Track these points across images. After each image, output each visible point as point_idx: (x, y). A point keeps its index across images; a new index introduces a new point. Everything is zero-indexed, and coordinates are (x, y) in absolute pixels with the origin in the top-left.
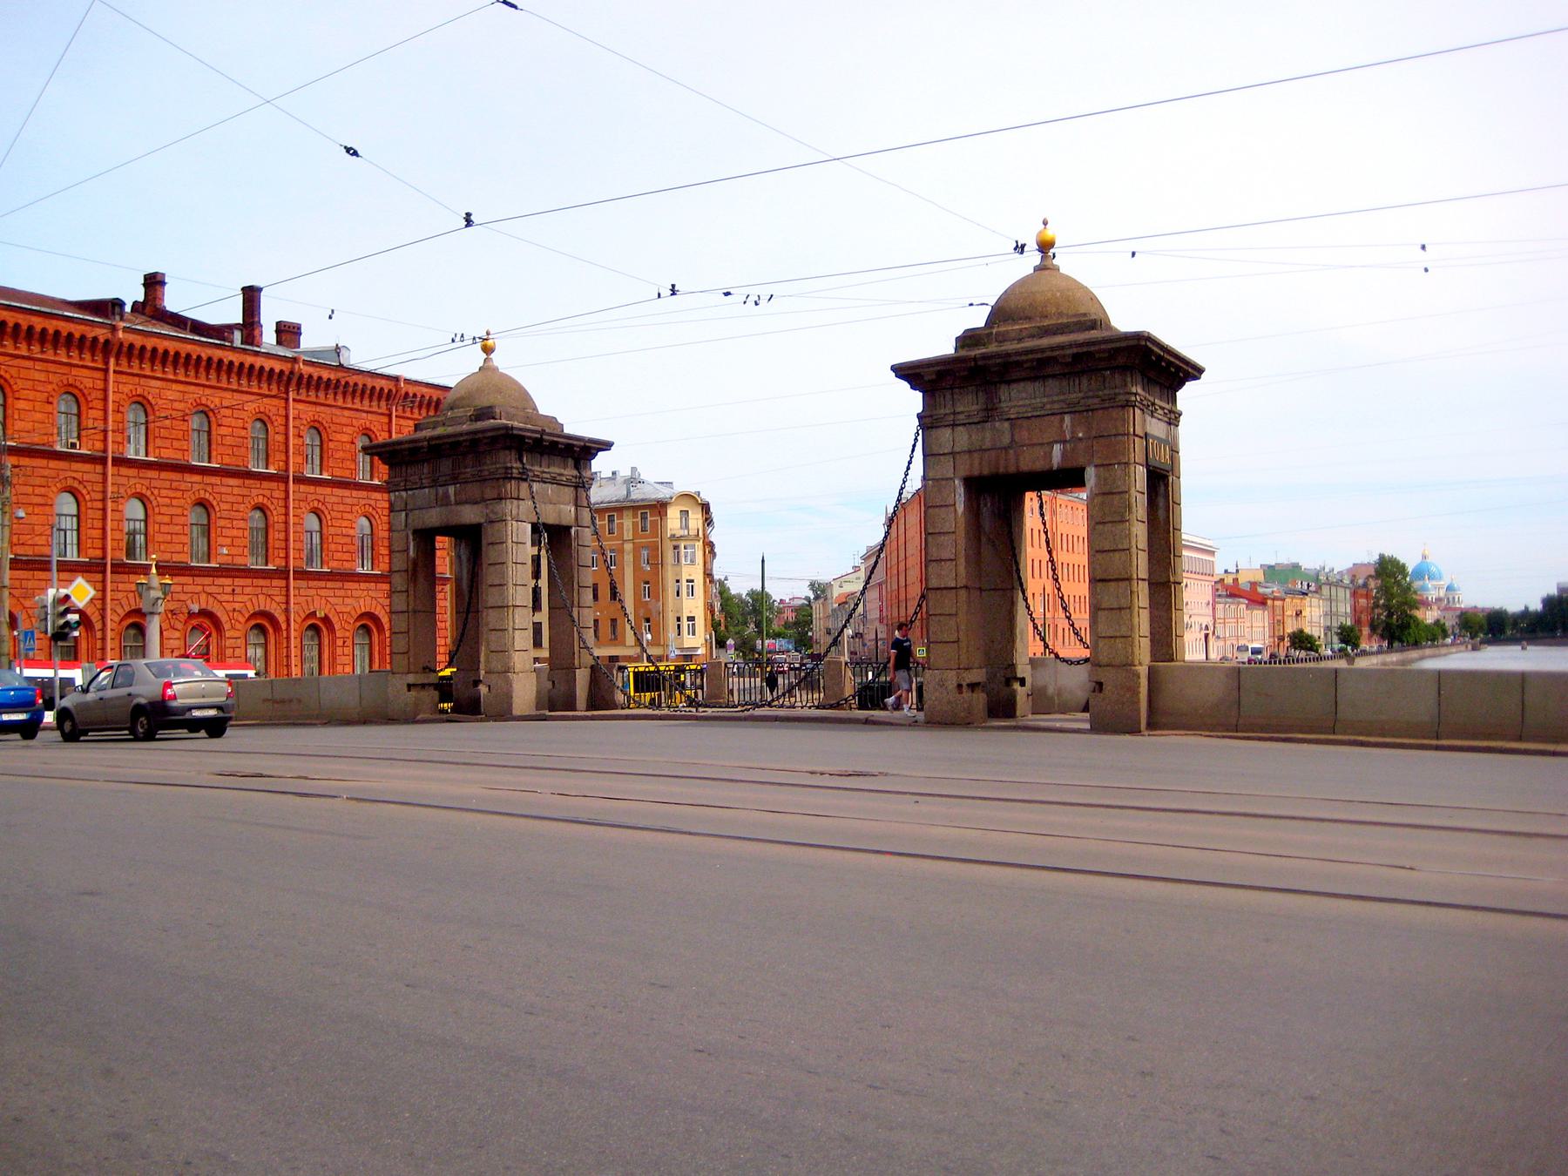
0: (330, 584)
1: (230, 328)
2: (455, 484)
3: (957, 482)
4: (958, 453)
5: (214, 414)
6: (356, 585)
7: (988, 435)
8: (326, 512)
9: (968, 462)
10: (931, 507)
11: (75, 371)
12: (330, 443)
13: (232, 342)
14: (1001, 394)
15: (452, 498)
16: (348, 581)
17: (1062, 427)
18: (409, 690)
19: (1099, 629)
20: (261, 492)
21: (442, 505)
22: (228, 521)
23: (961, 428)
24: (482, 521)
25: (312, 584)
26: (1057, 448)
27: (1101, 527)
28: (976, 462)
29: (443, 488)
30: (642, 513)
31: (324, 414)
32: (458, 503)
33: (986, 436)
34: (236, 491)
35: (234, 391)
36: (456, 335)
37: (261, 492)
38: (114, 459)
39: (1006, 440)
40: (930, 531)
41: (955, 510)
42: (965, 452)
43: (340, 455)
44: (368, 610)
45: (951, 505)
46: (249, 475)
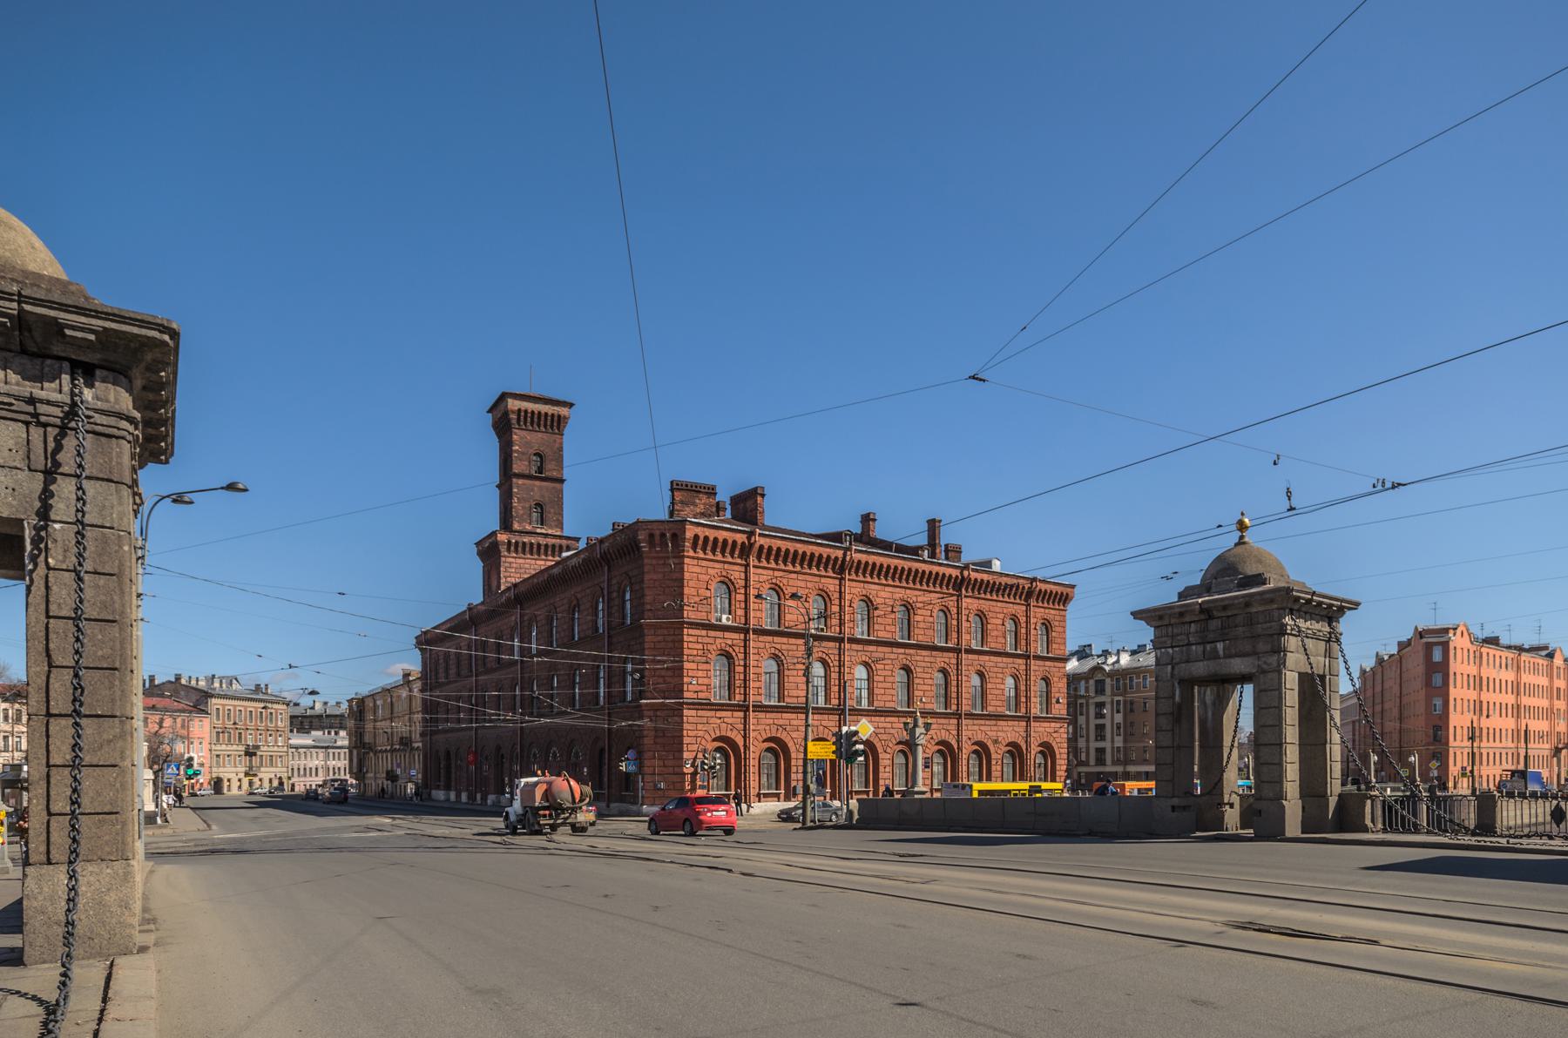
0: (987, 722)
1: (921, 548)
2: (1223, 641)
11: (823, 580)
13: (922, 556)
15: (1221, 653)
18: (1173, 811)
21: (1209, 659)
24: (1254, 671)
31: (985, 605)
34: (927, 659)
35: (924, 590)
36: (1378, 480)
37: (943, 659)
38: (849, 639)
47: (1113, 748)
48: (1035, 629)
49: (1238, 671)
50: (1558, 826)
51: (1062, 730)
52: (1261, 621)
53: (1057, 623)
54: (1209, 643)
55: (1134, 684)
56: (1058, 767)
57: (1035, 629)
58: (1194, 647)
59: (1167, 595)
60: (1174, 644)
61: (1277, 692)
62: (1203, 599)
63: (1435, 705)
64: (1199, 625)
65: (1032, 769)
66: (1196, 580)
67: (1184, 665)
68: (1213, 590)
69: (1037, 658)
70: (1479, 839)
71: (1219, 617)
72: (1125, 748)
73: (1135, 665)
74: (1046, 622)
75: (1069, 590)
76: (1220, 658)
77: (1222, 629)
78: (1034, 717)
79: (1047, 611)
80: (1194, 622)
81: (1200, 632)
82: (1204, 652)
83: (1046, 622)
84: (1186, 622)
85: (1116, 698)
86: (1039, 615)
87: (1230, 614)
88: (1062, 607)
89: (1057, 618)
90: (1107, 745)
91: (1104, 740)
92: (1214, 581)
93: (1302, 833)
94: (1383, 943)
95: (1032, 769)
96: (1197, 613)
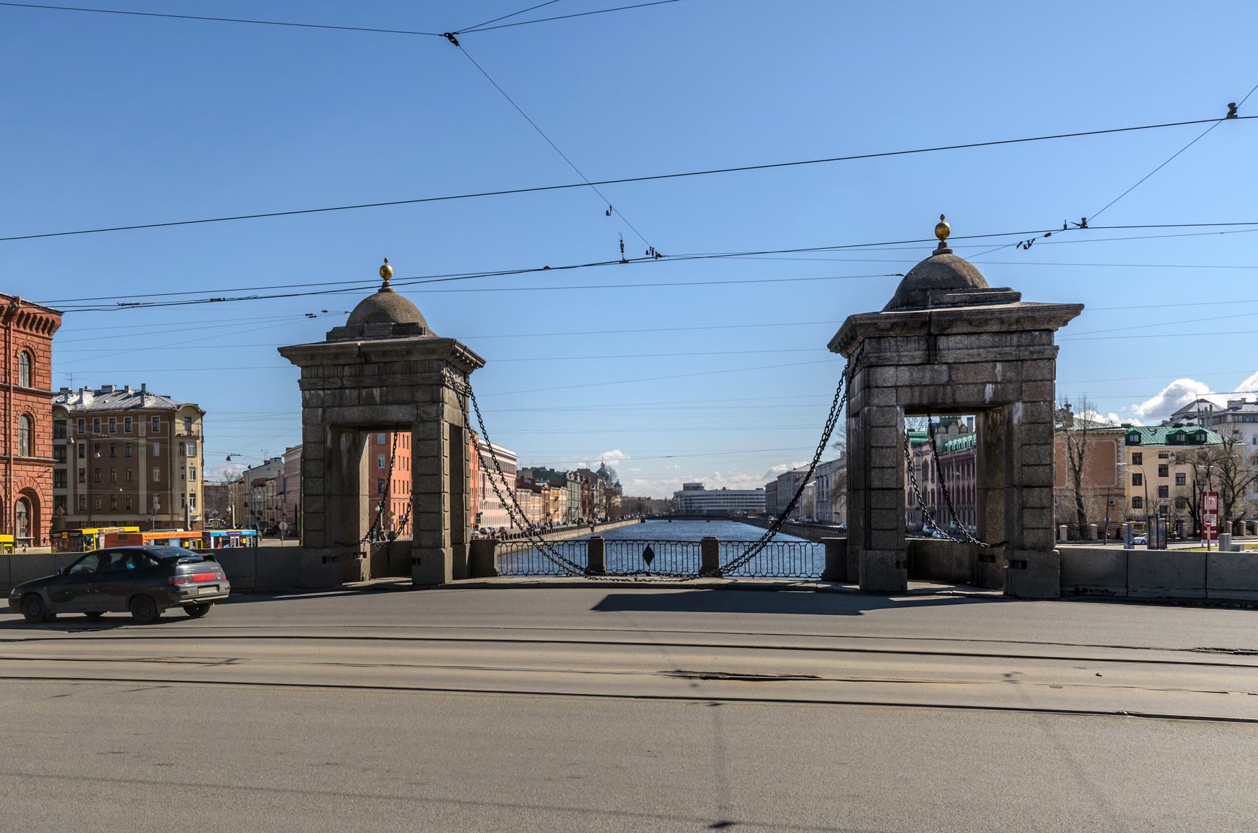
2: (381, 387)
4: (900, 386)
7: (928, 374)
9: (909, 394)
15: (378, 399)
19: (1024, 523)
21: (364, 405)
24: (412, 419)
26: (989, 389)
27: (1027, 447)
28: (917, 394)
29: (367, 390)
32: (384, 403)
33: (927, 375)
39: (944, 378)
42: (906, 386)
45: (893, 426)
47: (75, 495)
48: (16, 357)
49: (395, 419)
50: (649, 565)
51: (47, 475)
52: (420, 370)
53: (41, 353)
54: (364, 388)
55: (115, 427)
56: (42, 517)
57: (16, 357)
58: (348, 391)
59: (315, 334)
60: (326, 387)
61: (436, 442)
62: (363, 342)
63: (380, 461)
64: (353, 369)
65: (13, 519)
66: (342, 322)
67: (336, 409)
68: (367, 334)
69: (19, 390)
70: (613, 578)
71: (375, 363)
72: (90, 496)
73: (101, 407)
74: (28, 350)
75: (54, 316)
76: (377, 405)
77: (379, 375)
78: (14, 459)
79: (29, 337)
80: (348, 365)
81: (356, 376)
82: (359, 397)
83: (28, 350)
84: (340, 365)
86: (19, 342)
87: (387, 361)
88: (46, 335)
89: (41, 347)
90: (68, 492)
91: (66, 487)
92: (366, 325)
93: (454, 579)
94: (824, 677)
95: (13, 519)
96: (355, 356)
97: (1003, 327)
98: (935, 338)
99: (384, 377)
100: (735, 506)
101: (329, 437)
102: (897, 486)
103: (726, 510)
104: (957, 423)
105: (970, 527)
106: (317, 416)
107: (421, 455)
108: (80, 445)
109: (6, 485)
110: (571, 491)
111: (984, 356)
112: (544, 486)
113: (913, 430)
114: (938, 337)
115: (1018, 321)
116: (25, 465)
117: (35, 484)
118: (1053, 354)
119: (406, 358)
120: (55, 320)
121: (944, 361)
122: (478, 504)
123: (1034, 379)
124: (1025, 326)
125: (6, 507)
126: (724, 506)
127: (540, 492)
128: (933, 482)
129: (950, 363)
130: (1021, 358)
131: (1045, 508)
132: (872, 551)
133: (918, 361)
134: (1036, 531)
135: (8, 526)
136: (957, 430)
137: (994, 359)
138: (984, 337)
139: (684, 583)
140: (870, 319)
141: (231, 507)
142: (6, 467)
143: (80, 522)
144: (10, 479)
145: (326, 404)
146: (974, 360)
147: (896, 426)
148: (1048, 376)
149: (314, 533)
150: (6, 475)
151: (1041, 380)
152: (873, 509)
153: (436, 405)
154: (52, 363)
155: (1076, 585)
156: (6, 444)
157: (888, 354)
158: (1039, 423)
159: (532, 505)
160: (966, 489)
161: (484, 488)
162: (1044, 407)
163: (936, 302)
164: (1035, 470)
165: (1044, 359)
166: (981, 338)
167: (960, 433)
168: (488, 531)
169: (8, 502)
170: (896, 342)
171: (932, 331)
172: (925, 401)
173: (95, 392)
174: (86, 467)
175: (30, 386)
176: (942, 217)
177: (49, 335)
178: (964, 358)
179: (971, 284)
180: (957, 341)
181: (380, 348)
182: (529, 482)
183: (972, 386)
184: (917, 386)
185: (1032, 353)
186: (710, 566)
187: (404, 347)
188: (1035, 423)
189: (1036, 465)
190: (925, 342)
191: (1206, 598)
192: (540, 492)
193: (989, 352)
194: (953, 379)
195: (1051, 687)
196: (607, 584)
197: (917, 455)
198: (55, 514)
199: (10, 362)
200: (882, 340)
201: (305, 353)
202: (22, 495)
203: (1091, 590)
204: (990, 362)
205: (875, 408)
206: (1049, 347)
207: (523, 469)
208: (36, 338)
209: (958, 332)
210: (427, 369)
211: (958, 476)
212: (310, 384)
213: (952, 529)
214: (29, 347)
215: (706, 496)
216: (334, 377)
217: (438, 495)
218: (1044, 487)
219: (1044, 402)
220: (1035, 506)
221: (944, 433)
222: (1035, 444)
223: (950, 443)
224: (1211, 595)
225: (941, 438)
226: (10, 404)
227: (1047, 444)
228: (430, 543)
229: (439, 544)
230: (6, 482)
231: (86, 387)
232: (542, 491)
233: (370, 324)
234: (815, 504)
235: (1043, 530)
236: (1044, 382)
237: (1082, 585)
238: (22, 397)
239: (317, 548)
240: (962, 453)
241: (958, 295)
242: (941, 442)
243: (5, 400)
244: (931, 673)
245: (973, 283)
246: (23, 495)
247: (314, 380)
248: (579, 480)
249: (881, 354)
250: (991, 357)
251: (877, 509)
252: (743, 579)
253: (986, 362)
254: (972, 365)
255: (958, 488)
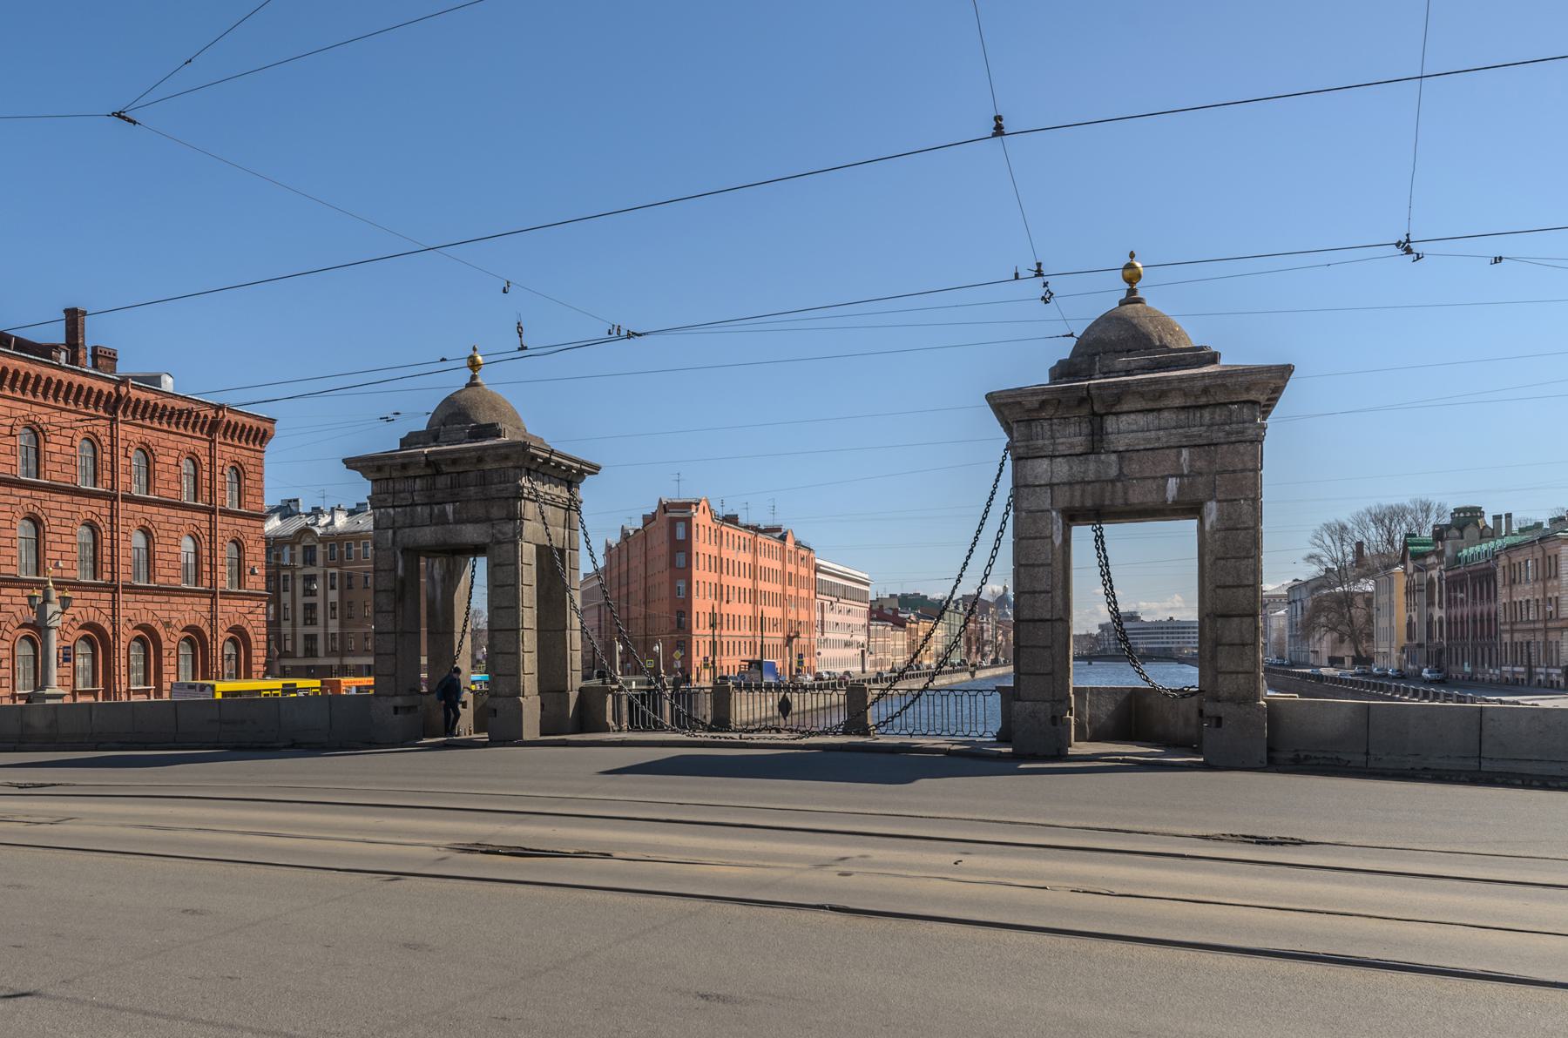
0: (156, 598)
2: (454, 502)
3: (1054, 513)
4: (1058, 484)
5: (44, 435)
6: (180, 600)
7: (1092, 466)
8: (153, 530)
9: (1067, 494)
10: (1023, 538)
12: (157, 465)
14: (1108, 426)
15: (451, 517)
16: (174, 596)
17: (1179, 461)
19: (1219, 665)
20: (90, 508)
21: (436, 524)
22: (57, 535)
23: (1059, 459)
24: (488, 541)
25: (139, 597)
26: (1172, 483)
27: (1223, 562)
28: (1078, 493)
29: (439, 506)
30: (330, 545)
32: (456, 522)
33: (1091, 468)
34: (65, 507)
37: (90, 508)
39: (1113, 472)
40: (1023, 563)
41: (1053, 543)
42: (1064, 484)
43: (166, 476)
44: (193, 623)
45: (1047, 538)
46: (77, 492)
47: (326, 634)
48: (222, 474)
50: (785, 719)
51: (260, 610)
53: (251, 468)
54: (437, 504)
56: (254, 660)
57: (222, 474)
58: (419, 509)
59: (386, 441)
61: (513, 567)
62: (430, 449)
64: (425, 481)
65: (219, 662)
67: (407, 530)
68: (441, 439)
71: (448, 473)
72: (342, 634)
75: (267, 425)
77: (451, 488)
79: (238, 451)
80: (420, 477)
82: (431, 515)
84: (411, 477)
85: (331, 570)
86: (227, 456)
88: (258, 447)
89: (252, 461)
90: (318, 630)
91: (316, 624)
92: (442, 427)
95: (219, 662)
96: (422, 465)
97: (1188, 401)
98: (1102, 419)
99: (456, 491)
100: (1184, 642)
101: (400, 564)
102: (1052, 616)
103: (1170, 649)
104: (1477, 525)
105: (1491, 671)
106: (387, 539)
107: (497, 584)
108: (284, 576)
109: (212, 623)
110: (950, 624)
111: (1164, 440)
112: (909, 618)
113: (1414, 535)
114: (1105, 417)
115: (1206, 391)
116: (234, 599)
117: (246, 621)
118: (1257, 435)
119: (480, 467)
120: (268, 429)
121: (1112, 449)
122: (814, 642)
123: (1231, 469)
124: (1217, 398)
125: (212, 649)
126: (1168, 643)
127: (904, 626)
128: (1441, 608)
129: (1120, 452)
130: (1215, 441)
131: (1247, 644)
132: (1020, 703)
133: (1079, 450)
134: (1234, 676)
135: (215, 670)
136: (1477, 534)
137: (1179, 444)
138: (1166, 414)
139: (798, 742)
140: (1011, 396)
141: (659, 646)
142: (212, 602)
143: (331, 666)
144: (216, 616)
145: (396, 525)
146: (1152, 446)
147: (1051, 537)
148: (1250, 465)
149: (385, 678)
150: (212, 611)
151: (1242, 471)
152: (1023, 647)
153: (512, 522)
154: (265, 480)
155: (1296, 751)
156: (211, 576)
157: (1040, 442)
158: (1237, 529)
159: (892, 643)
160: (1459, 620)
161: (822, 621)
162: (1245, 507)
163: (1105, 370)
164: (1233, 593)
165: (1245, 442)
166: (1161, 416)
167: (1481, 537)
168: (826, 676)
169: (214, 643)
170: (1051, 425)
171: (1095, 408)
172: (1089, 503)
173: (349, 510)
174: (337, 601)
175: (239, 508)
176: (1132, 255)
177: (261, 446)
178: (1138, 444)
179: (1158, 343)
180: (1130, 421)
181: (449, 456)
182: (891, 613)
183: (1150, 481)
184: (1078, 483)
185: (1228, 434)
186: (856, 723)
187: (473, 453)
188: (1233, 529)
189: (1233, 587)
190: (1088, 424)
191: (1480, 771)
192: (904, 626)
193: (1171, 435)
194: (1125, 472)
195: (839, 875)
196: (700, 742)
197: (1417, 569)
198: (268, 656)
199: (215, 480)
200: (1033, 424)
201: (371, 464)
202: (186, 634)
203: (1316, 758)
204: (1174, 447)
205: (1024, 514)
206: (1251, 425)
207: (890, 595)
208: (245, 451)
209: (1130, 409)
210: (503, 479)
211: (1462, 599)
212: (379, 501)
213: (1467, 672)
214: (237, 462)
215: (1143, 629)
216: (404, 491)
217: (515, 632)
218: (1030, 621)
219: (1245, 500)
220: (1233, 642)
221: (1456, 538)
222: (1234, 558)
223: (1465, 552)
224: (1486, 766)
225: (1454, 546)
226: (215, 529)
227: (1248, 558)
228: (507, 690)
229: (517, 692)
230: (211, 619)
231: (339, 506)
232: (908, 625)
233: (448, 427)
234: (1287, 639)
235: (1243, 676)
236: (1244, 474)
237: (1304, 750)
238: (230, 520)
239: (388, 696)
240: (1480, 567)
241: (1135, 360)
242: (1453, 550)
243: (211, 525)
244: (705, 852)
245: (1161, 342)
246: (232, 635)
247: (383, 495)
248: (961, 609)
249: (1031, 442)
250: (1173, 441)
251: (1026, 647)
252: (676, 735)
253: (1168, 448)
254: (1150, 452)
255: (1475, 616)
